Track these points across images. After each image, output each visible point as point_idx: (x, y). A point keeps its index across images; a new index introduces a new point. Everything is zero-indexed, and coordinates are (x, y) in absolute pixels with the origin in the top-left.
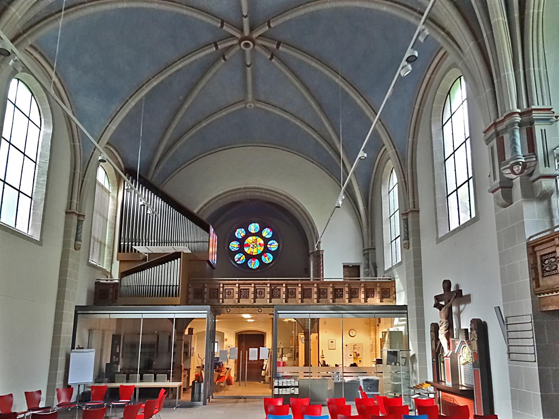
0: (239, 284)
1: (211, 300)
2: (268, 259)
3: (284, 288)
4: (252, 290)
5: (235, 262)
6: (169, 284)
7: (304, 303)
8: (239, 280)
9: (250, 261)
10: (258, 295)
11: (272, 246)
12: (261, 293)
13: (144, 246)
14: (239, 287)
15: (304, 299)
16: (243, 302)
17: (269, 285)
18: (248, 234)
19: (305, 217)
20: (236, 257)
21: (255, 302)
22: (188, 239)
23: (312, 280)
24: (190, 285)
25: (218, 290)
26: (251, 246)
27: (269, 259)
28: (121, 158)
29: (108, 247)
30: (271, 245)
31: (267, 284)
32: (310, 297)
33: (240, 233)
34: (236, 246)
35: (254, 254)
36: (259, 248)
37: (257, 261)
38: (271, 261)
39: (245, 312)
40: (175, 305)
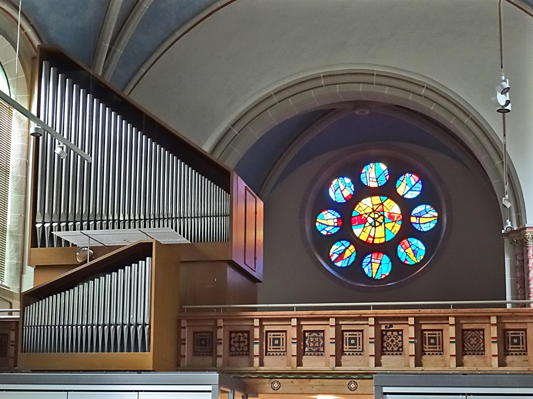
0: (299, 320)
1: (234, 359)
2: (413, 252)
3: (412, 329)
4: (331, 333)
5: (332, 264)
6: (126, 321)
7: (465, 368)
8: (298, 309)
9: (367, 260)
10: (346, 347)
11: (422, 220)
12: (277, 342)
13: (78, 232)
14: (299, 326)
15: (466, 358)
16: (311, 363)
17: (372, 321)
18: (362, 191)
19: (484, 140)
20: (332, 250)
21: (338, 364)
22: (179, 207)
23: (509, 306)
24: (184, 323)
25: (249, 333)
26: (370, 220)
27: (415, 253)
28: (32, 26)
29: (11, 236)
30: (418, 217)
31: (367, 319)
32: (480, 351)
33: (340, 189)
34: (331, 223)
35: (377, 241)
36: (389, 226)
37: (385, 259)
38: (421, 256)
39: (314, 390)
40: (139, 371)
